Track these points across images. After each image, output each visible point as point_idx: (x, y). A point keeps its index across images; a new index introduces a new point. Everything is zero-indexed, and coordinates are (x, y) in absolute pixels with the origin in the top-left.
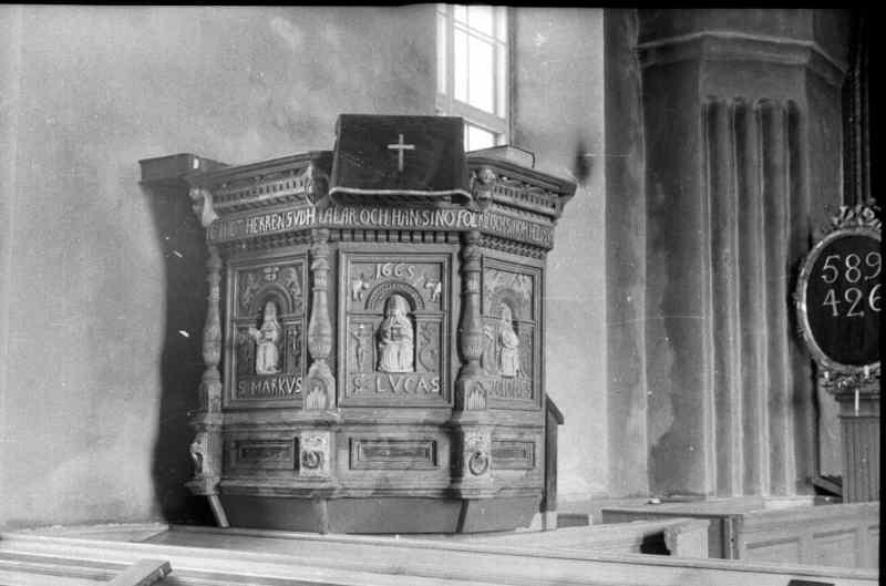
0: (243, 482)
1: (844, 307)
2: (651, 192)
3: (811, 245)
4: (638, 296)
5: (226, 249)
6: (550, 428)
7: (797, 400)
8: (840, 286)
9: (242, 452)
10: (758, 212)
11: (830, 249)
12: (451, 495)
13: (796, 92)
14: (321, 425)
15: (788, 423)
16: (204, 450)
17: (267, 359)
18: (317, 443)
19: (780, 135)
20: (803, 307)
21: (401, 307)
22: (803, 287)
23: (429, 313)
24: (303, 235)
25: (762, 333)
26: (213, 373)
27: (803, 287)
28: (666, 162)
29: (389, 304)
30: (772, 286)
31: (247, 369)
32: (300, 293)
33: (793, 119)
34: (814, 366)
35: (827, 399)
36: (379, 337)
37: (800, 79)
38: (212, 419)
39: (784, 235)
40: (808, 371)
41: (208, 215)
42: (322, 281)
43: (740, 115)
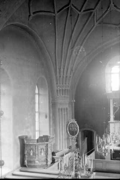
0: (29, 164)
1: (72, 130)
2: (53, 117)
3: (69, 123)
4: (51, 129)
5: (27, 145)
6: (44, 145)
7: (67, 139)
8: (72, 128)
9: (29, 162)
10: (63, 119)
11: (71, 124)
12: (47, 164)
13: (67, 106)
14: (37, 160)
15: (66, 141)
16: (26, 161)
17: (32, 154)
18: (37, 162)
19: (66, 110)
20: (68, 129)
21: (42, 150)
22: (68, 127)
23: (45, 150)
24: (36, 145)
25: (64, 133)
26: (26, 155)
27: (68, 127)
28: (54, 114)
29: (41, 150)
30: (65, 127)
31: (29, 154)
32: (35, 149)
33: (67, 109)
34: (69, 135)
35: (70, 139)
36: (41, 152)
37: (68, 105)
38: (27, 159)
39: (66, 121)
40: (68, 136)
41: (26, 142)
42: (37, 149)
43: (62, 109)
